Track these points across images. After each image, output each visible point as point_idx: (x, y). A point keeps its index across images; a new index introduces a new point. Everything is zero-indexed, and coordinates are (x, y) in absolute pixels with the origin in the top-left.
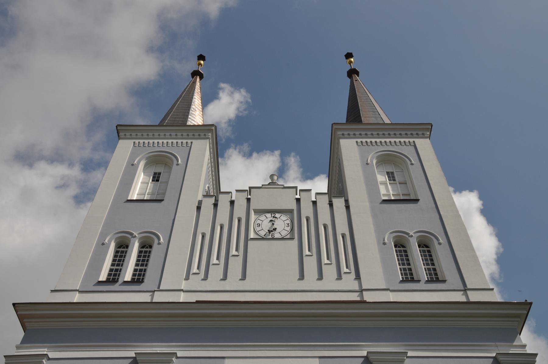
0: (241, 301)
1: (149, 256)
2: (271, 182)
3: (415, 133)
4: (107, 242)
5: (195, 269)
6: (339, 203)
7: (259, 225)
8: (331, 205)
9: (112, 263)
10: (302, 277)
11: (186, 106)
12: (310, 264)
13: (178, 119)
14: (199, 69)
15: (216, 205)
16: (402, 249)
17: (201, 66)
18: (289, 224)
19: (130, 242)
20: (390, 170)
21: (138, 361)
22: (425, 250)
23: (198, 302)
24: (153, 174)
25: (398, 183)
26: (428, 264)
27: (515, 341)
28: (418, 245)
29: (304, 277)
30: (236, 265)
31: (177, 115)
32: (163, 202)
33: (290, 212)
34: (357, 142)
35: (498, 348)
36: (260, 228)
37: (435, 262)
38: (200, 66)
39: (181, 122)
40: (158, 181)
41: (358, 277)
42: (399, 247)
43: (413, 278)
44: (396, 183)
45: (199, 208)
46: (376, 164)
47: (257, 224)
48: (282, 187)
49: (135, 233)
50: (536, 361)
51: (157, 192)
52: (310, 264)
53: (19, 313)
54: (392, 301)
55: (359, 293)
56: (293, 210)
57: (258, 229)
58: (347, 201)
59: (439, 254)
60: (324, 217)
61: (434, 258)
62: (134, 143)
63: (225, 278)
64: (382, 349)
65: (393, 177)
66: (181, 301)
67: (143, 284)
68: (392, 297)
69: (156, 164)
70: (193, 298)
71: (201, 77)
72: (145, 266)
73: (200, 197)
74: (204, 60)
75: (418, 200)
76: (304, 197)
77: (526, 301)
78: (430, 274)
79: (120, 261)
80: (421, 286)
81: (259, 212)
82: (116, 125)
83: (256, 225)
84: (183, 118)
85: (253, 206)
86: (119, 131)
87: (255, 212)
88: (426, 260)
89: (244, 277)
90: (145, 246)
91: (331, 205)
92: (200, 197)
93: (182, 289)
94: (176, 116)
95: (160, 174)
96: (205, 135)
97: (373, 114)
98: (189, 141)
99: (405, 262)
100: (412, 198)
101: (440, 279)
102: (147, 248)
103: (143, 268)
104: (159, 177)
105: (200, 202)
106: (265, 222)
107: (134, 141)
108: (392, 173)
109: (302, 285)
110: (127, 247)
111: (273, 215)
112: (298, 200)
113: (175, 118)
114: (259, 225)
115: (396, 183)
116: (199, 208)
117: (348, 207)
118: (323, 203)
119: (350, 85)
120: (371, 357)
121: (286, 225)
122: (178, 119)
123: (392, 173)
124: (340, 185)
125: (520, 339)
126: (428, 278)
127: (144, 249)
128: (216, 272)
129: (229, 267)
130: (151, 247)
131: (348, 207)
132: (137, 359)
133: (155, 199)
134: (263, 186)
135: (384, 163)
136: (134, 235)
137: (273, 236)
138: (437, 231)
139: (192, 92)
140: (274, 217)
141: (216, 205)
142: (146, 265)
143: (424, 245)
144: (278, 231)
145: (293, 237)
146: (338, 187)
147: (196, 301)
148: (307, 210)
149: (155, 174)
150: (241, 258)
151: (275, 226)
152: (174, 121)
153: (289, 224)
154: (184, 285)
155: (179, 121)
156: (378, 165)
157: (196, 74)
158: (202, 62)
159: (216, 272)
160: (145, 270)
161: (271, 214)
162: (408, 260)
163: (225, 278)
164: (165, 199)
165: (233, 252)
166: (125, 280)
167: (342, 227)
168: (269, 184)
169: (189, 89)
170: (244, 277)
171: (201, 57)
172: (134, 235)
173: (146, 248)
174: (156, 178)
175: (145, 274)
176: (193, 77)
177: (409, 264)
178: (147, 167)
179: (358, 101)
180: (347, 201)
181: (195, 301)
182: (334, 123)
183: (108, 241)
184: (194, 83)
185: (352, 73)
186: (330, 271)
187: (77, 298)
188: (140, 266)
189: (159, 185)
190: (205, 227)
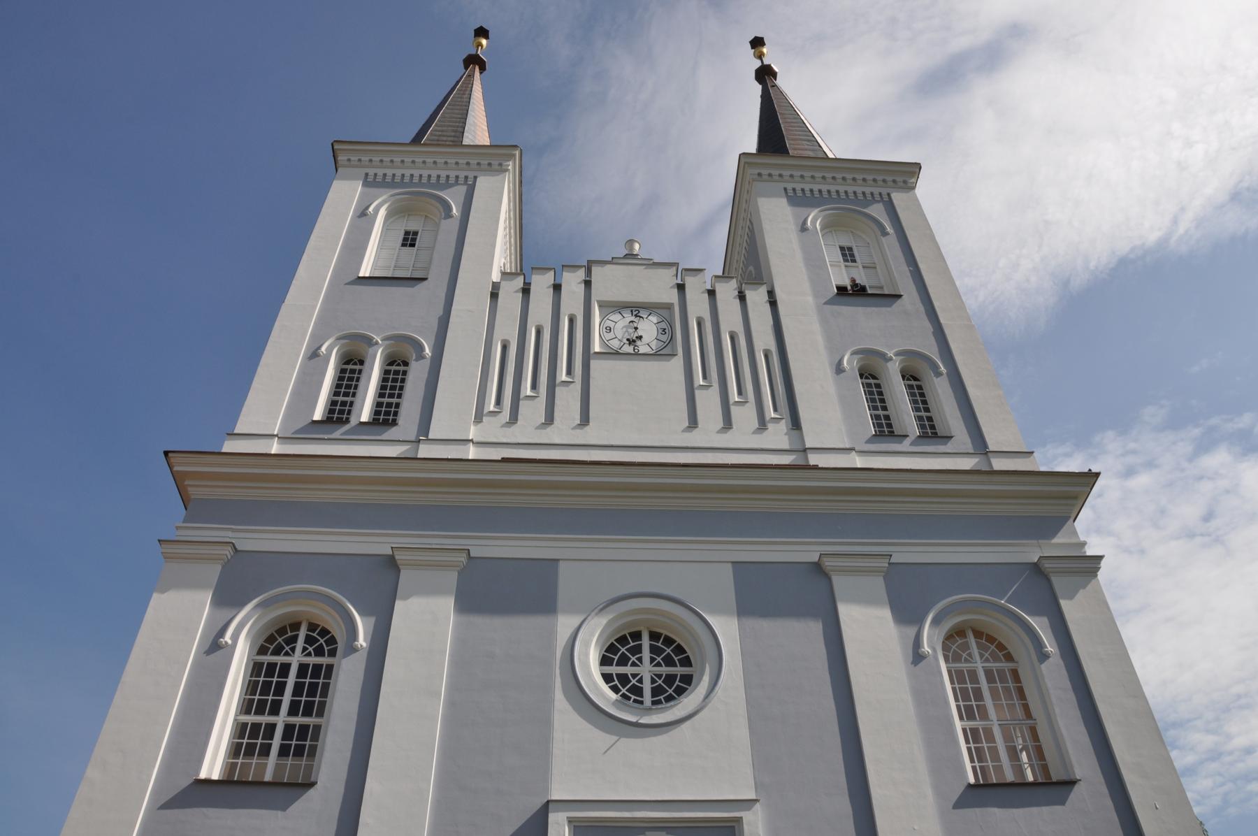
0: (587, 461)
1: (403, 381)
2: (627, 253)
3: (902, 180)
4: (325, 352)
5: (491, 405)
6: (756, 297)
7: (609, 330)
8: (742, 297)
9: (382, 385)
10: (693, 422)
11: (459, 116)
12: (709, 402)
13: (445, 138)
14: (479, 52)
15: (526, 291)
16: (872, 381)
17: (482, 48)
18: (665, 329)
19: (367, 354)
20: (846, 244)
21: (399, 562)
22: (913, 385)
23: (504, 460)
24: (402, 233)
25: (861, 267)
26: (875, 408)
27: (1059, 535)
28: (860, 374)
29: (588, 422)
30: (568, 400)
31: (442, 131)
32: (425, 283)
33: (669, 307)
34: (785, 189)
35: (1041, 549)
36: (611, 335)
37: (931, 405)
38: (480, 48)
39: (452, 139)
40: (413, 245)
41: (796, 424)
42: (867, 378)
43: (936, 433)
44: (857, 267)
45: (494, 295)
46: (821, 230)
47: (606, 328)
48: (651, 262)
49: (375, 337)
50: (1100, 568)
51: (412, 265)
52: (709, 402)
53: (176, 469)
54: (859, 466)
55: (977, 460)
56: (672, 304)
57: (608, 336)
58: (771, 293)
59: (940, 391)
60: (730, 318)
61: (929, 398)
62: (367, 175)
63: (550, 419)
64: (778, 540)
65: (852, 255)
66: (470, 458)
67: (394, 429)
68: (859, 462)
69: (409, 215)
70: (496, 454)
71: (483, 68)
72: (397, 398)
73: (496, 277)
74: (487, 37)
75: (900, 296)
76: (690, 282)
77: (1090, 470)
78: (880, 425)
79: (348, 387)
80: (905, 445)
81: (611, 307)
82: (332, 141)
83: (604, 330)
84: (454, 136)
85: (596, 295)
86: (338, 152)
87: (600, 306)
88: (873, 400)
89: (585, 420)
90: (395, 361)
91: (742, 297)
92: (496, 277)
93: (470, 438)
94: (440, 133)
95: (416, 233)
96: (500, 165)
97: (808, 145)
98: (471, 175)
99: (879, 404)
100: (886, 293)
101: (896, 434)
102: (399, 365)
103: (394, 400)
104: (414, 240)
105: (496, 286)
106: (620, 322)
107: (367, 170)
108: (850, 249)
109: (695, 439)
110: (362, 362)
111: (634, 313)
112: (681, 288)
113: (440, 136)
114: (609, 330)
115: (857, 267)
116: (494, 295)
117: (773, 303)
118: (726, 292)
119: (760, 93)
120: (1047, 566)
121: (660, 331)
122: (445, 138)
123: (850, 249)
124: (751, 268)
125: (1075, 533)
126: (875, 431)
127: (394, 367)
128: (533, 411)
129: (556, 401)
130: (406, 364)
131: (773, 303)
132: (397, 557)
133: (409, 276)
134: (615, 261)
135: (835, 231)
136: (375, 340)
137: (636, 351)
138: (932, 351)
139: (467, 92)
140: (636, 316)
141: (526, 291)
142: (400, 396)
143: (911, 376)
144: (645, 339)
145: (673, 352)
146: (745, 273)
147: (502, 458)
148: (698, 306)
149: (407, 233)
150: (577, 386)
151: (640, 333)
152: (438, 141)
153: (665, 329)
154: (473, 432)
155: (446, 141)
156: (825, 231)
157: (474, 61)
158: (484, 42)
159: (533, 411)
160: (398, 405)
161: (632, 311)
162: (883, 401)
163: (550, 419)
164: (429, 277)
165: (562, 376)
166: (361, 420)
167: (764, 339)
168: (626, 256)
169: (461, 86)
170: (585, 420)
171: (482, 32)
172: (375, 340)
173: (396, 366)
174: (409, 240)
175: (397, 411)
176: (466, 68)
177: (885, 408)
178: (391, 220)
179: (781, 122)
180: (771, 293)
181: (500, 459)
182: (744, 153)
183: (326, 350)
184: (471, 76)
185: (765, 74)
186: (745, 416)
187: (275, 448)
188: (388, 398)
189: (415, 252)
190: (507, 329)
